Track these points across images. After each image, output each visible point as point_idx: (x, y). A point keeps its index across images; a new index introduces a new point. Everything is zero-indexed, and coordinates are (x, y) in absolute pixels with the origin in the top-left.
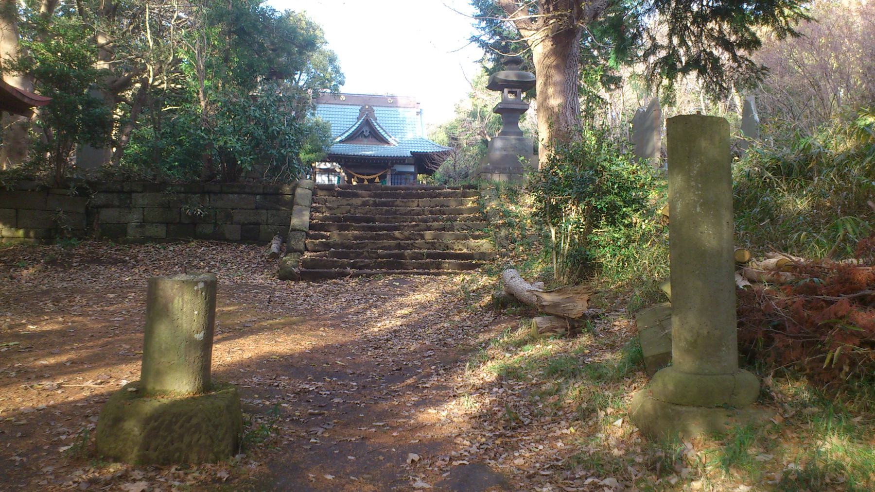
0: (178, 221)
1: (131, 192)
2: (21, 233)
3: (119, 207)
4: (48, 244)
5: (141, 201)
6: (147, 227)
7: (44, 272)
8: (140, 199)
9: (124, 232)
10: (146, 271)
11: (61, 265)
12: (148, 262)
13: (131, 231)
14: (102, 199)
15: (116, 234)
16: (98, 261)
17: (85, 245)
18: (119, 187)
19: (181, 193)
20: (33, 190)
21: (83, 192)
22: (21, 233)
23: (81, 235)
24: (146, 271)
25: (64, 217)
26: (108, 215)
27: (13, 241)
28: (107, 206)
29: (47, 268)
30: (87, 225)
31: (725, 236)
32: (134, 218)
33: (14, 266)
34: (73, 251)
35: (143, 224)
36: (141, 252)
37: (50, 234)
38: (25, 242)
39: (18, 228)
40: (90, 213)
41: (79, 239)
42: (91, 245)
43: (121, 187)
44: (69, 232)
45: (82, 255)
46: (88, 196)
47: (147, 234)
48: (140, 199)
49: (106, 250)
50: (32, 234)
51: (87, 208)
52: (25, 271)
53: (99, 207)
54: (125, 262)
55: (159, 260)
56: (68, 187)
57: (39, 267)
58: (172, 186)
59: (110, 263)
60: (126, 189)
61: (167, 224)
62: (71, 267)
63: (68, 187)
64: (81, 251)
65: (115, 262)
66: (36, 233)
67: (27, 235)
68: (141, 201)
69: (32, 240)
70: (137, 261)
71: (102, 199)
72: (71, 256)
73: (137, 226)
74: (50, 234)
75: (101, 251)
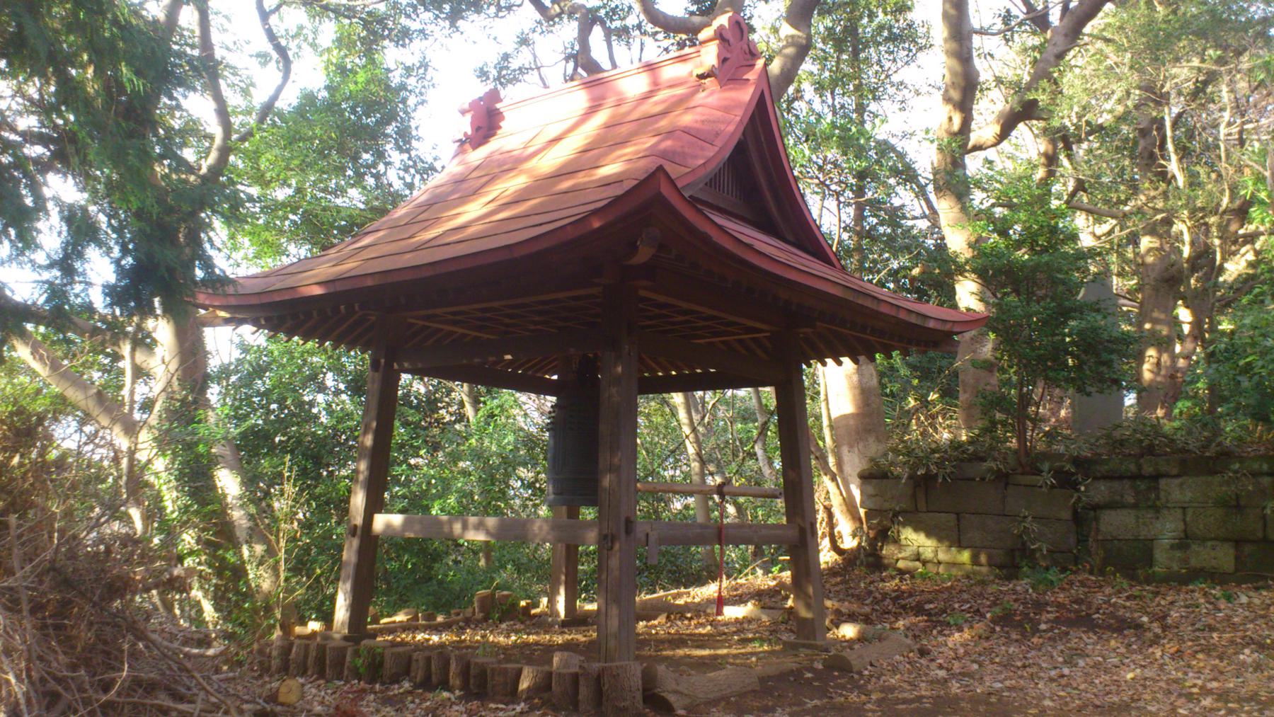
0: (1260, 535)
1: (1156, 477)
2: (965, 556)
3: (1135, 506)
4: (1009, 578)
5: (1177, 495)
6: (1194, 547)
7: (987, 638)
8: (1177, 491)
9: (1149, 560)
10: (1178, 655)
11: (1020, 625)
12: (1186, 629)
13: (1160, 556)
14: (1101, 492)
15: (1132, 562)
16: (1085, 622)
17: (1071, 583)
18: (1133, 467)
19: (1261, 474)
20: (983, 479)
21: (1066, 481)
22: (965, 556)
23: (1067, 560)
24: (1178, 655)
25: (1035, 527)
26: (1115, 523)
27: (954, 571)
28: (1113, 505)
29: (993, 631)
30: (1079, 541)
31: (609, 169)
32: (1166, 529)
33: (942, 623)
34: (1049, 597)
35: (1184, 542)
36: (1176, 605)
37: (1012, 561)
38: (974, 573)
39: (961, 547)
40: (1082, 518)
41: (1064, 570)
42: (1083, 584)
43: (1142, 464)
44: (1044, 557)
45: (1060, 606)
46: (1075, 486)
47: (1194, 562)
48: (1177, 491)
49: (1113, 596)
50: (983, 559)
51: (1075, 513)
52: (957, 635)
53: (1097, 507)
54: (1139, 627)
55: (1212, 629)
56: (1039, 472)
57: (980, 627)
58: (1241, 459)
59: (1109, 628)
60: (1148, 469)
61: (1238, 542)
62: (1035, 631)
63: (1039, 472)
64: (1061, 597)
65: (1121, 626)
66: (990, 558)
67: (975, 560)
68: (1177, 495)
69: (984, 570)
70: (1165, 628)
71: (1101, 492)
72: (1040, 606)
73: (1172, 547)
74: (1012, 561)
75: (1099, 598)
